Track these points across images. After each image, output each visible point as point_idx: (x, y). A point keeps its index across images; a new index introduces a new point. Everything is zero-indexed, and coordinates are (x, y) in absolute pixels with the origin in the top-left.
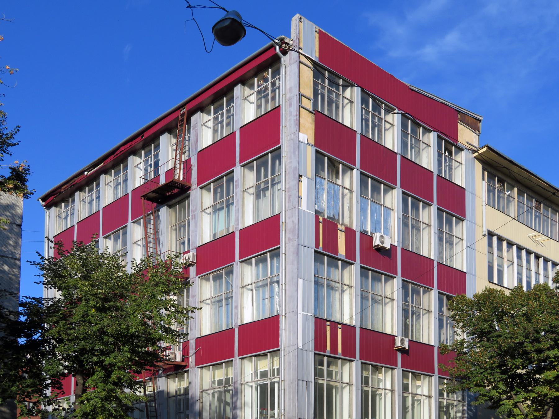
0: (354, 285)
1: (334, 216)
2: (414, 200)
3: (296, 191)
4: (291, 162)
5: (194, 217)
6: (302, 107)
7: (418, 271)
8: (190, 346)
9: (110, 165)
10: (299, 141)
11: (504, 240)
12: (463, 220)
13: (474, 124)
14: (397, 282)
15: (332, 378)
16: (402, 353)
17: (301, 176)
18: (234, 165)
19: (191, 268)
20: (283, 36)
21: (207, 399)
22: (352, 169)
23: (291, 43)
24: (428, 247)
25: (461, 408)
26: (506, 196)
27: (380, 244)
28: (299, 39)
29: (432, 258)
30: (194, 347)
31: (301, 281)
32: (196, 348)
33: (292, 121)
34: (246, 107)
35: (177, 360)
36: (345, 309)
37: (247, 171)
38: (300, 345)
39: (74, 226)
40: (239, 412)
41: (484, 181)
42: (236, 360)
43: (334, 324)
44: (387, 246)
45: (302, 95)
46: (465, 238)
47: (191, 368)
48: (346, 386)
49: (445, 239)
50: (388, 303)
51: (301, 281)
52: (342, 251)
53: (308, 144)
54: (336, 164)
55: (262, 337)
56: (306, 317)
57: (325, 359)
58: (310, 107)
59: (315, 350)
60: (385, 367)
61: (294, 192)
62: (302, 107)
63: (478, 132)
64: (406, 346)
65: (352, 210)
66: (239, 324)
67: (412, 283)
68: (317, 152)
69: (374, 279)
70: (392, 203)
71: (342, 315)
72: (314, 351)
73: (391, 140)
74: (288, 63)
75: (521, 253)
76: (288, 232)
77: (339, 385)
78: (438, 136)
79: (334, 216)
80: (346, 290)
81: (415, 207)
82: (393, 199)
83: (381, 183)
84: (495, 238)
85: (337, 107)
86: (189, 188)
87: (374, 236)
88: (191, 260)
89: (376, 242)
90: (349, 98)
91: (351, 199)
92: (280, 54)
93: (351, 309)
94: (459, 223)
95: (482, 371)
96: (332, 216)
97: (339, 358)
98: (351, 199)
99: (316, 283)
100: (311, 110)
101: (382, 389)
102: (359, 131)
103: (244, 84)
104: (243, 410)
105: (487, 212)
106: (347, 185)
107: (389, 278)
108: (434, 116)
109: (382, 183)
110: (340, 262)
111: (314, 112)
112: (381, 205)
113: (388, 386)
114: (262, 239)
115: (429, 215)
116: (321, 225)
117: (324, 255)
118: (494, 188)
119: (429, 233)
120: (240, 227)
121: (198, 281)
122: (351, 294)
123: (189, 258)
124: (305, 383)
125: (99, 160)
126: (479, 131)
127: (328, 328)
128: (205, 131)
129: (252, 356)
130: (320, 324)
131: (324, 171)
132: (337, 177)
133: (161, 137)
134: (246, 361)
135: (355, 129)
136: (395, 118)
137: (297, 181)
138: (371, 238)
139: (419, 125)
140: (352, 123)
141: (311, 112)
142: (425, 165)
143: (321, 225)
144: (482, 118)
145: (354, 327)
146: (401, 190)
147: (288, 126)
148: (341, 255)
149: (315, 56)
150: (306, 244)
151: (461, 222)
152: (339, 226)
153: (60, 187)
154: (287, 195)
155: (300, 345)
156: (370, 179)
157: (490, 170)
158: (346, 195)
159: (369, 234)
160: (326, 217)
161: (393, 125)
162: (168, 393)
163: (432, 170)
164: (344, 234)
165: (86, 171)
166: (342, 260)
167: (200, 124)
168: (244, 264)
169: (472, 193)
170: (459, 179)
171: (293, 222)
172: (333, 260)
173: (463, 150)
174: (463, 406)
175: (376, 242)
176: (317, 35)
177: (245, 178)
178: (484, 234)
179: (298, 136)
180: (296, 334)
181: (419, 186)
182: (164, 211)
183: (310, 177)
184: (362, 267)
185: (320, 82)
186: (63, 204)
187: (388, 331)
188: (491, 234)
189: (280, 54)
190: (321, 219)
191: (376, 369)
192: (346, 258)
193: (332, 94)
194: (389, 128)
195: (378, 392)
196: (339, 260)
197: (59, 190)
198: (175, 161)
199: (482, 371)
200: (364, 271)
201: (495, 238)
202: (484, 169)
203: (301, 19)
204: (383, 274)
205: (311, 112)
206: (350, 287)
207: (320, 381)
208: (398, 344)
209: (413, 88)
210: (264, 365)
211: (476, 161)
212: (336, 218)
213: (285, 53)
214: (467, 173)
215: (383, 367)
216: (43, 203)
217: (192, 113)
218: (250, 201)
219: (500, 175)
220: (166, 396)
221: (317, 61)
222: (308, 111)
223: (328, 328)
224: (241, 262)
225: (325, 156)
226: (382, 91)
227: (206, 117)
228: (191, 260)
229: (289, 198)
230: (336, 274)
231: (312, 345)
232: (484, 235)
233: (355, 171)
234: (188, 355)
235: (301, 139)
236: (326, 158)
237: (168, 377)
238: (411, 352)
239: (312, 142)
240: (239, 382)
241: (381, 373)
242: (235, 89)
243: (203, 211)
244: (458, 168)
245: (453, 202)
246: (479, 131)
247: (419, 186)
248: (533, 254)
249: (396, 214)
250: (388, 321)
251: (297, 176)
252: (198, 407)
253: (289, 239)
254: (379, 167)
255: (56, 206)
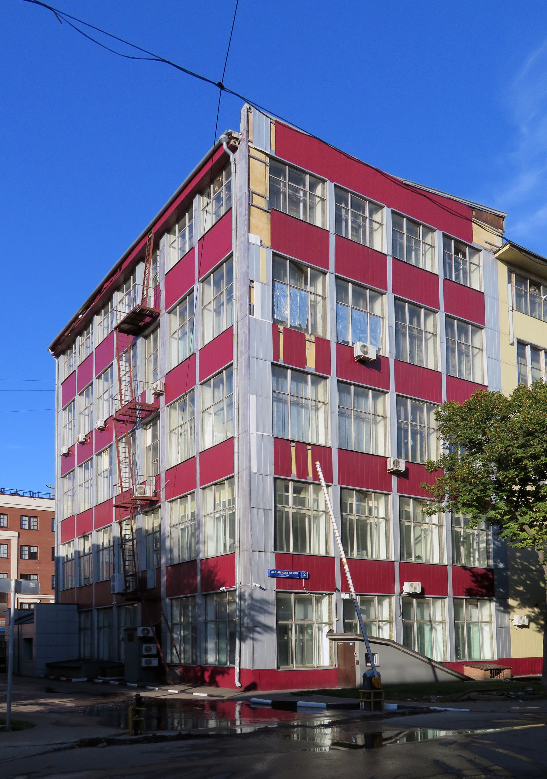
0: (329, 401)
1: (300, 325)
2: (412, 307)
3: (250, 302)
4: (241, 267)
5: (163, 344)
6: (252, 206)
7: (417, 384)
8: (161, 480)
9: (100, 304)
10: (249, 243)
11: (541, 350)
12: (482, 329)
13: (496, 222)
14: (390, 398)
15: (304, 505)
16: (398, 477)
17: (253, 282)
18: (194, 282)
19: (161, 397)
20: (230, 131)
21: (177, 533)
22: (325, 273)
23: (240, 137)
24: (433, 356)
25: (485, 538)
26: (543, 300)
27: (362, 354)
28: (248, 131)
29: (439, 370)
30: (164, 480)
31: (253, 398)
32: (166, 481)
33: (242, 222)
34: (204, 215)
35: (147, 495)
36: (320, 428)
37: (206, 286)
38: (254, 469)
39: (75, 371)
40: (201, 547)
41: (510, 285)
42: (198, 491)
43: (302, 446)
44: (372, 356)
45: (252, 193)
46: (484, 348)
47: (162, 502)
48: (322, 515)
49: (456, 349)
50: (380, 421)
51: (253, 398)
52: (311, 364)
53: (262, 245)
54: (304, 268)
55: (217, 464)
56: (261, 439)
57: (290, 484)
58: (265, 206)
59: (275, 474)
60: (375, 493)
61: (245, 299)
62: (252, 206)
63: (501, 231)
64: (402, 468)
65: (326, 319)
66: (200, 451)
67: (411, 399)
68: (274, 254)
69: (357, 395)
70: (382, 311)
71: (317, 435)
72: (273, 475)
73: (381, 241)
74: (237, 160)
75: (524, 350)
76: (240, 345)
77: (312, 514)
78: (444, 235)
79: (300, 325)
80: (320, 408)
81: (414, 314)
82: (384, 305)
83: (366, 288)
84: (528, 348)
85: (465, 274)
86: (158, 315)
87: (355, 346)
88: (158, 388)
89: (358, 352)
90: (320, 195)
91: (324, 306)
92: (228, 151)
93: (326, 428)
94: (477, 332)
95: (471, 487)
96: (297, 325)
97: (311, 483)
98: (324, 306)
99: (341, 414)
100: (266, 208)
101: (428, 524)
102: (390, 253)
103: (202, 194)
104: (206, 545)
105: (508, 317)
106: (320, 291)
107: (379, 393)
108: (456, 222)
109: (367, 289)
110: (309, 376)
111: (270, 211)
112: (367, 313)
113: (382, 514)
114: (217, 358)
115: (435, 323)
116: (281, 335)
117: (288, 368)
118: (526, 293)
119: (435, 343)
120: (200, 347)
121: (167, 410)
122: (326, 412)
123: (156, 387)
124: (261, 511)
125: (88, 301)
126: (503, 230)
127: (293, 450)
128: (171, 251)
129: (212, 485)
130: (281, 446)
131: (286, 276)
132: (306, 283)
133: (137, 267)
134: (207, 491)
135: (328, 229)
136: (384, 216)
137: (248, 287)
138: (352, 348)
139: (419, 225)
140: (324, 223)
141: (265, 211)
142: (428, 268)
143: (281, 335)
144: (506, 215)
145: (330, 449)
146: (393, 296)
147: (238, 229)
148: (310, 368)
149: (272, 150)
150: (260, 356)
151: (480, 331)
152: (307, 337)
153: (62, 335)
154: (239, 304)
155: (254, 469)
156: (350, 284)
157: (519, 272)
158: (319, 302)
159: (351, 345)
160: (289, 327)
161: (381, 225)
162: (147, 531)
163: (437, 274)
164: (313, 344)
165: (80, 314)
166: (312, 374)
167: (167, 247)
168: (204, 387)
169: (495, 299)
170: (476, 282)
171: (244, 332)
172: (300, 374)
173: (481, 251)
174: (487, 535)
175: (358, 352)
176: (273, 127)
177: (204, 293)
178: (511, 342)
179: (253, 240)
180: (254, 460)
181: (415, 290)
182: (140, 341)
183: (265, 282)
184: (339, 381)
185: (343, 205)
186: (68, 351)
187: (381, 453)
188: (521, 344)
189: (228, 151)
190: (281, 328)
191: (363, 495)
192: (317, 371)
193: (359, 219)
194: (378, 228)
195: (368, 521)
196: (308, 373)
197: (63, 338)
198: (144, 288)
199: (471, 487)
200: (343, 386)
201: (528, 348)
202: (510, 272)
203: (250, 108)
204: (370, 389)
205: (265, 211)
206: (325, 404)
207: (407, 524)
208: (391, 466)
209: (408, 183)
210: (224, 494)
211: (499, 263)
212: (304, 327)
213: (234, 149)
214: (488, 276)
215: (373, 492)
216: (53, 352)
217: (159, 236)
218: (209, 317)
219: (533, 278)
220: (144, 533)
221: (274, 155)
222: (262, 209)
223: (293, 450)
224: (202, 384)
225: (287, 259)
226: (362, 183)
227: (172, 237)
228: (158, 388)
229: (241, 307)
230: (307, 389)
231: (271, 469)
232: (512, 344)
233: (328, 275)
234: (160, 489)
235: (250, 241)
236: (288, 261)
237: (146, 513)
238: (411, 475)
239: (268, 242)
240: (201, 514)
241: (371, 500)
242: (194, 201)
243: (171, 336)
244: (476, 271)
245: (468, 310)
246: (503, 230)
247: (415, 290)
248: (529, 346)
249: (387, 322)
250: (381, 442)
251: (247, 281)
252: (168, 544)
253: (241, 352)
254: (361, 271)
255: (64, 354)
